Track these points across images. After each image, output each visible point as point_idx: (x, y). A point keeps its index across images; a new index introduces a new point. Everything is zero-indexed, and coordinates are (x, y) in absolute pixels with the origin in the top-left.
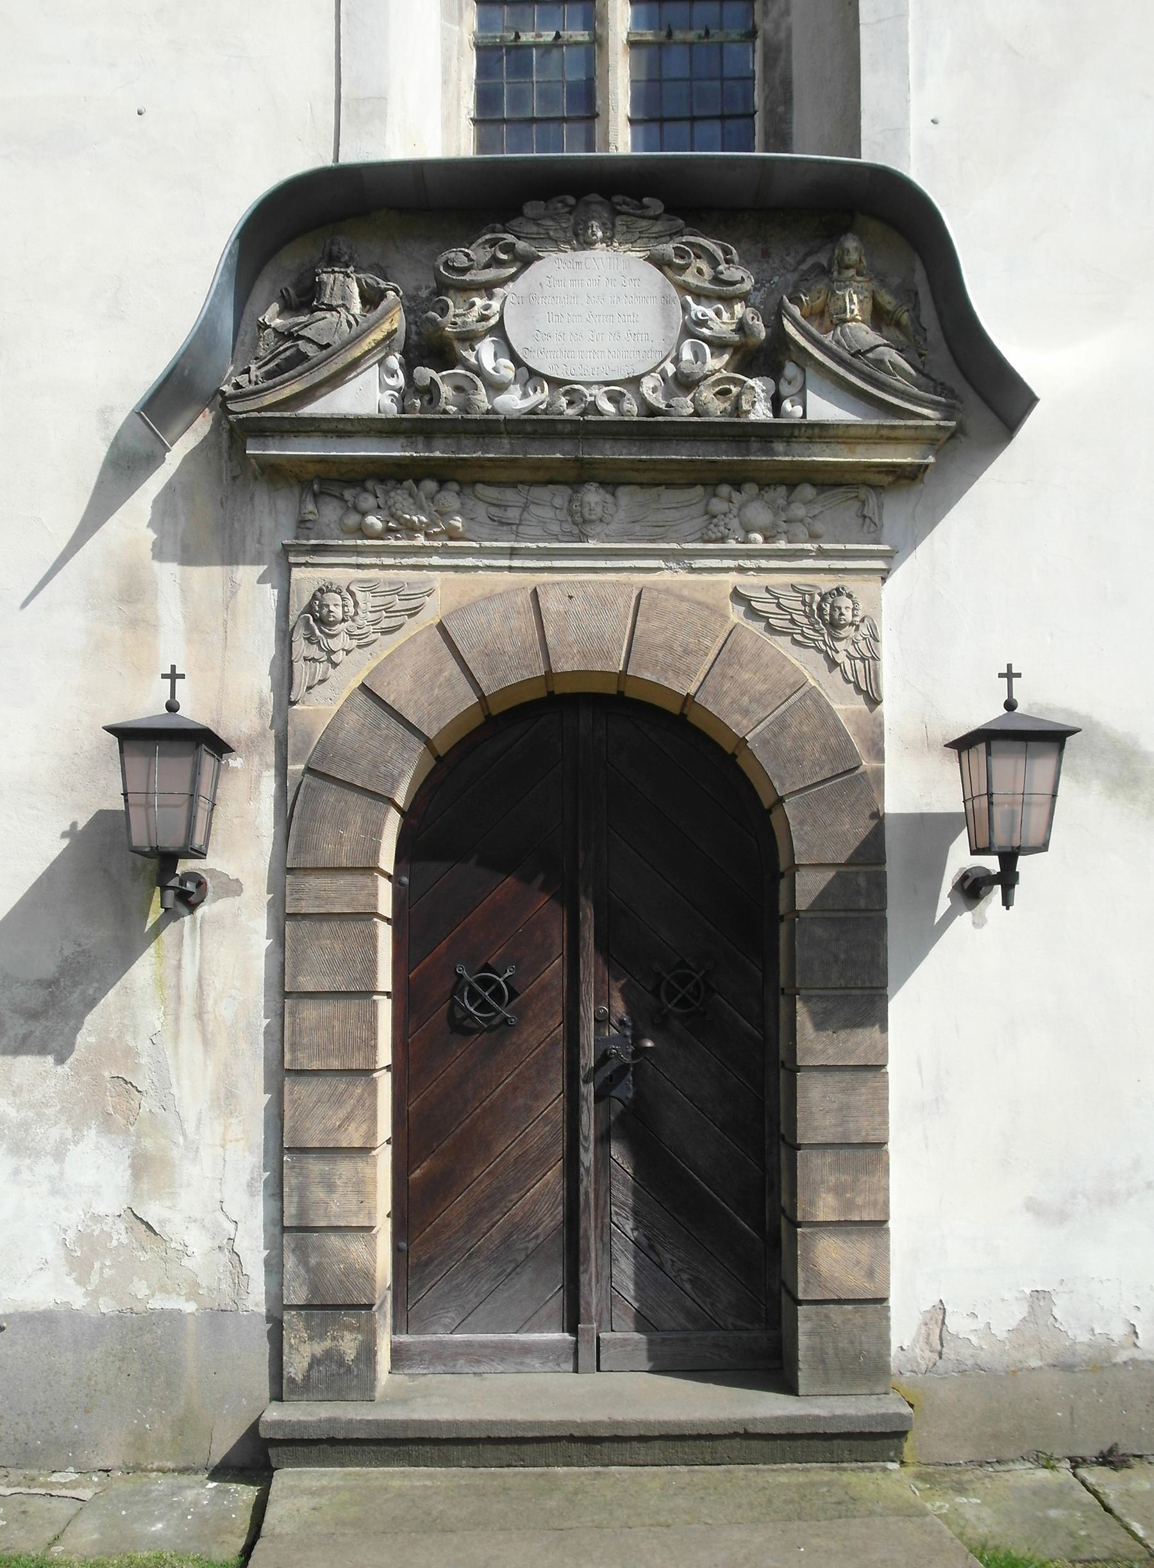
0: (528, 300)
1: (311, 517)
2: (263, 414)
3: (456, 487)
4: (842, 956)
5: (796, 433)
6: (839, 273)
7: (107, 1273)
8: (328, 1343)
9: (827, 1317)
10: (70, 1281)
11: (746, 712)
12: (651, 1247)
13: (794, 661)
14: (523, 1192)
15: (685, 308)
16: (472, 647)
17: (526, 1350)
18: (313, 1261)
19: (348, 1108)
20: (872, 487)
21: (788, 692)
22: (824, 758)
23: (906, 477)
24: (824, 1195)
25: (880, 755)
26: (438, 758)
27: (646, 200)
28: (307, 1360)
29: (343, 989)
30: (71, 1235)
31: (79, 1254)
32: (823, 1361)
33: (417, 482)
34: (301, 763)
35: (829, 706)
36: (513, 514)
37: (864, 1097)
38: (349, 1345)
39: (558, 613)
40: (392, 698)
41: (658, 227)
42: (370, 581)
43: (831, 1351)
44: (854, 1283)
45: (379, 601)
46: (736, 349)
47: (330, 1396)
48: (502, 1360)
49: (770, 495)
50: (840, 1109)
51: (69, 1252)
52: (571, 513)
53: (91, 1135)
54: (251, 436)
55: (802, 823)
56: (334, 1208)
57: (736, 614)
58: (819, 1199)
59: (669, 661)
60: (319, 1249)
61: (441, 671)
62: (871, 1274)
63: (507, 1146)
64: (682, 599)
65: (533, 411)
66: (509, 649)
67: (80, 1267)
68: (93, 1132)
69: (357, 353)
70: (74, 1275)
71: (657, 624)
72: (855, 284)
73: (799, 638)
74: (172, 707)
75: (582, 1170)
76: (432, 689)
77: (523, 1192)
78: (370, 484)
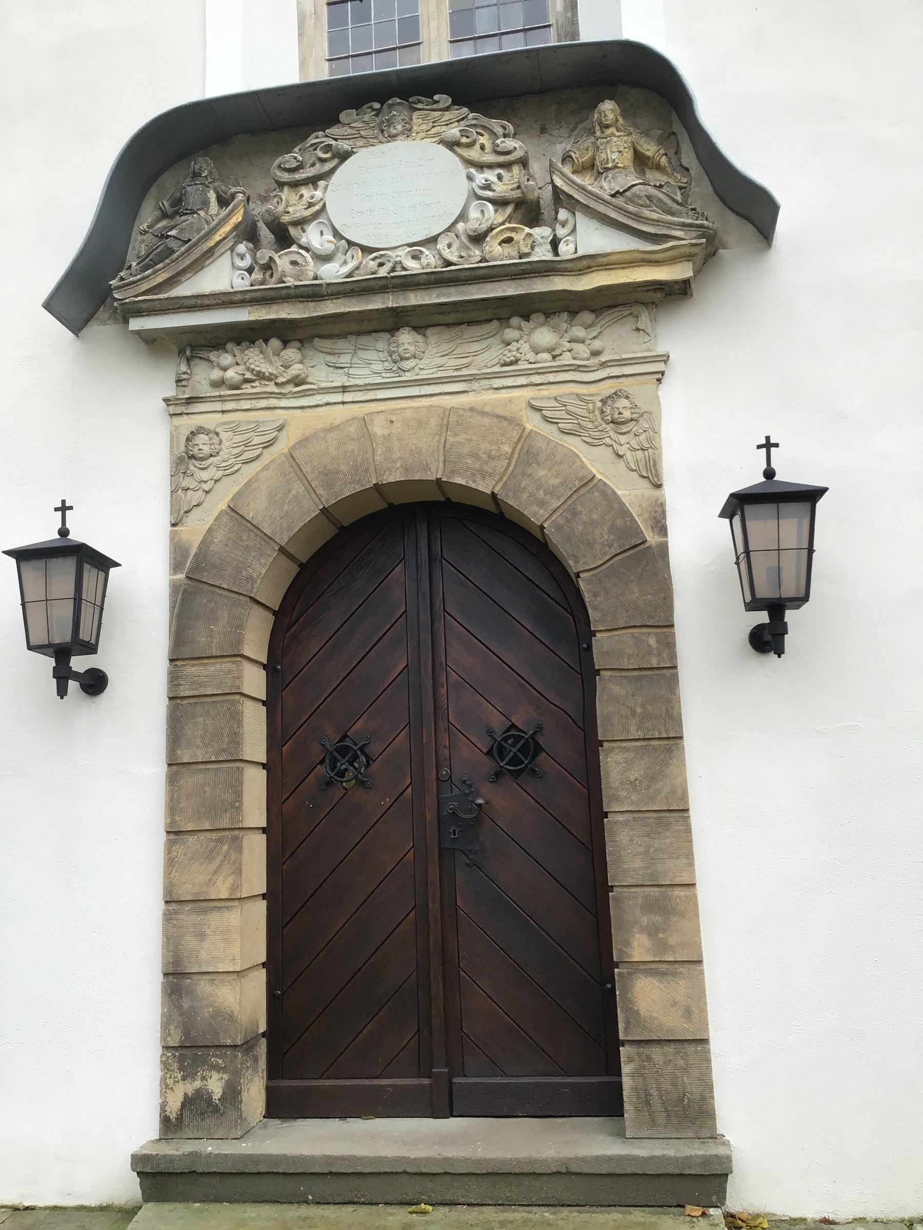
1: (185, 376)
3: (297, 344)
4: (639, 710)
6: (602, 132)
8: (198, 1084)
9: (649, 1058)
11: (542, 504)
13: (584, 459)
15: (470, 178)
21: (577, 484)
22: (612, 537)
23: (678, 292)
24: (637, 936)
25: (663, 530)
27: (436, 97)
28: (180, 1098)
29: (213, 759)
32: (648, 1103)
33: (266, 341)
34: (181, 573)
35: (614, 492)
37: (668, 841)
38: (215, 1085)
39: (383, 436)
40: (251, 515)
41: (448, 116)
42: (233, 422)
43: (654, 1093)
45: (238, 439)
49: (555, 320)
52: (391, 354)
54: (132, 317)
55: (595, 595)
56: (204, 955)
57: (532, 422)
58: (635, 946)
59: (478, 465)
60: (191, 992)
61: (289, 491)
62: (688, 1013)
64: (483, 414)
66: (344, 468)
69: (211, 243)
72: (615, 139)
76: (283, 506)
78: (229, 346)
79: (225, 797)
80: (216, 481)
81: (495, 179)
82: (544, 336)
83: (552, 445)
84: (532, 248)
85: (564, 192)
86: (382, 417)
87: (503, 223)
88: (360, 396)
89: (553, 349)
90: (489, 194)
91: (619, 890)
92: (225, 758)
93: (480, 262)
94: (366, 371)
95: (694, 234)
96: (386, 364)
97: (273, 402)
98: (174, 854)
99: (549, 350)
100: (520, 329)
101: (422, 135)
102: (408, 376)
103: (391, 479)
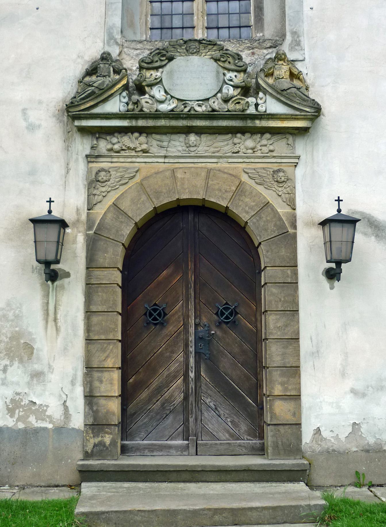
0: (171, 74)
1: (95, 146)
2: (80, 113)
3: (145, 135)
4: (282, 299)
5: (263, 117)
7: (21, 414)
8: (100, 439)
9: (279, 431)
10: (8, 416)
12: (216, 408)
14: (169, 388)
16: (151, 190)
17: (170, 447)
18: (95, 408)
19: (108, 353)
20: (291, 134)
21: (262, 205)
22: (275, 228)
25: (295, 227)
26: (138, 229)
28: (92, 445)
29: (106, 310)
30: (8, 401)
31: (11, 407)
32: (277, 446)
33: (132, 133)
36: (165, 144)
39: (181, 178)
44: (289, 418)
46: (242, 88)
47: (101, 458)
48: (162, 450)
49: (255, 137)
50: (283, 354)
51: (7, 406)
53: (16, 364)
55: (267, 252)
60: (97, 404)
63: (164, 373)
65: (172, 110)
67: (11, 411)
68: (17, 362)
69: (112, 91)
70: (9, 414)
71: (216, 182)
73: (266, 186)
74: (50, 212)
75: (190, 379)
77: (169, 388)
79: (111, 326)
80: (108, 192)
81: (234, 77)
82: (250, 143)
83: (252, 188)
84: (248, 107)
85: (263, 87)
86: (181, 170)
87: (237, 96)
88: (172, 160)
89: (254, 149)
90: (232, 83)
91: (271, 368)
92: (111, 310)
93: (227, 111)
94: (174, 150)
95: (313, 111)
96: (184, 148)
97: (134, 160)
98: (89, 349)
99: (253, 149)
100: (241, 139)
101: (204, 54)
102: (192, 154)
103: (185, 197)
